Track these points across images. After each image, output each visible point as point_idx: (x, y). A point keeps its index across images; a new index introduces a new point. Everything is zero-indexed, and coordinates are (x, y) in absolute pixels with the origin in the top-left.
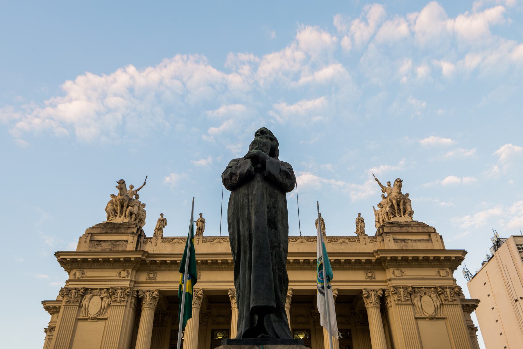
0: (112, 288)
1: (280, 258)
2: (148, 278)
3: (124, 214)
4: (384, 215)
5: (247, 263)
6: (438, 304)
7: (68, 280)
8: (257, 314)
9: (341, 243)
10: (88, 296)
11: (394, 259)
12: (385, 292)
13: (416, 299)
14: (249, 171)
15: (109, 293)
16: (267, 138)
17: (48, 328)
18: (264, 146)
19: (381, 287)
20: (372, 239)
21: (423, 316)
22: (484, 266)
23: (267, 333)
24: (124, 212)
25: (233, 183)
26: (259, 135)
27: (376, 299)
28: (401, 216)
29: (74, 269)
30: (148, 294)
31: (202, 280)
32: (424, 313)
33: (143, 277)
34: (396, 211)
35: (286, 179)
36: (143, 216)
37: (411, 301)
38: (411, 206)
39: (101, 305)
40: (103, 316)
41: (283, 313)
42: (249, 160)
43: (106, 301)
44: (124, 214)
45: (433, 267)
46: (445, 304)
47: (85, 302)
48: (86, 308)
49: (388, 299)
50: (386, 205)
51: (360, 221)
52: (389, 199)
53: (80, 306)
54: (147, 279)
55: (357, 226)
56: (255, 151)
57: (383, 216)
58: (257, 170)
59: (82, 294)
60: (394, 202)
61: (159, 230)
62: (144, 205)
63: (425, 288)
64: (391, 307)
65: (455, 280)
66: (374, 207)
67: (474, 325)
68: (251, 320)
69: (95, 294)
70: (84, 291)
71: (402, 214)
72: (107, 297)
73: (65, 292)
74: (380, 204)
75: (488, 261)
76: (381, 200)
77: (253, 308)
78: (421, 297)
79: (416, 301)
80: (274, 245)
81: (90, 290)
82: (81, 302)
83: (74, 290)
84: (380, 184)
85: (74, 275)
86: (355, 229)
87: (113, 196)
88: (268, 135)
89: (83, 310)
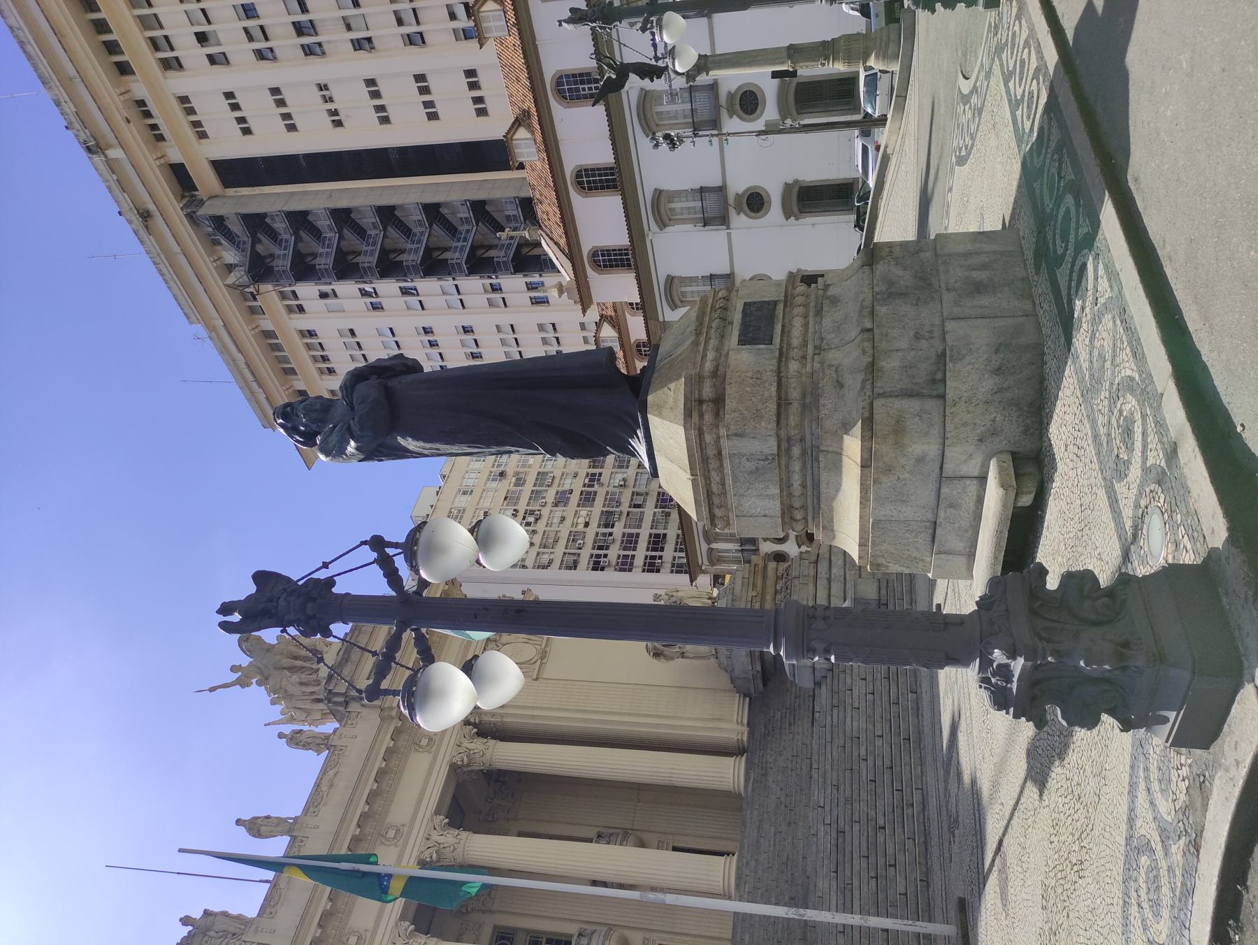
9: (331, 786)
30: (435, 837)
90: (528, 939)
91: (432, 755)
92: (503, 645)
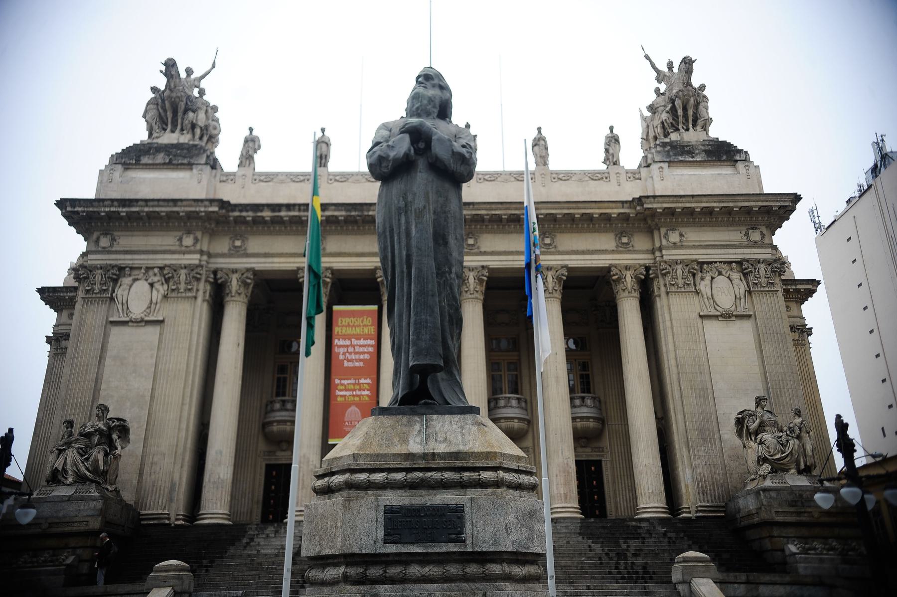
0: (169, 266)
1: (451, 289)
2: (232, 248)
3: (179, 127)
4: (657, 127)
5: (405, 299)
6: (742, 291)
7: (85, 250)
8: (418, 373)
10: (126, 281)
11: (671, 212)
12: (649, 271)
13: (703, 283)
14: (407, 155)
15: (164, 276)
16: (434, 86)
17: (52, 335)
18: (430, 104)
19: (642, 262)
20: (634, 175)
21: (713, 312)
22: (850, 205)
23: (432, 399)
24: (179, 121)
25: (384, 172)
26: (423, 83)
27: (633, 283)
28: (687, 130)
29: (94, 231)
31: (328, 250)
32: (716, 306)
33: (222, 245)
34: (681, 119)
35: (461, 164)
36: (215, 128)
37: (695, 285)
38: (707, 109)
39: (150, 297)
40: (155, 315)
41: (454, 368)
42: (407, 137)
43: (162, 289)
44: (179, 127)
45: (739, 224)
46: (753, 291)
47: (120, 292)
48: (124, 302)
49: (655, 283)
50: (663, 108)
51: (613, 141)
52: (667, 97)
53: (112, 299)
54: (230, 249)
55: (607, 151)
56: (415, 120)
57: (656, 129)
58: (418, 152)
59: (114, 277)
60: (678, 103)
61: (247, 158)
62: (215, 109)
63: (721, 262)
64: (659, 296)
65: (775, 248)
66: (641, 111)
67: (807, 325)
68: (410, 382)
69: (139, 277)
70: (118, 272)
71: (691, 126)
72: (161, 282)
73: (81, 272)
74: (650, 106)
75: (860, 197)
76: (653, 97)
77: (413, 366)
78: (713, 278)
79: (704, 286)
80: (443, 270)
81: (127, 269)
82: (113, 291)
83: (98, 269)
84: (653, 66)
85: (96, 242)
86: (602, 155)
87: (154, 90)
88: (436, 81)
89: (120, 307)
90: (586, 361)
91: (616, 249)
92: (728, 277)
